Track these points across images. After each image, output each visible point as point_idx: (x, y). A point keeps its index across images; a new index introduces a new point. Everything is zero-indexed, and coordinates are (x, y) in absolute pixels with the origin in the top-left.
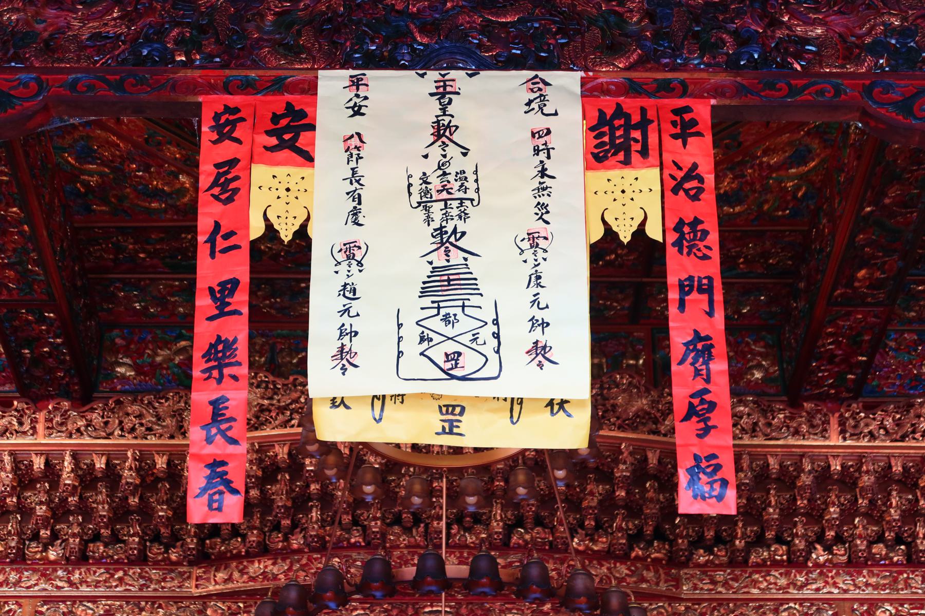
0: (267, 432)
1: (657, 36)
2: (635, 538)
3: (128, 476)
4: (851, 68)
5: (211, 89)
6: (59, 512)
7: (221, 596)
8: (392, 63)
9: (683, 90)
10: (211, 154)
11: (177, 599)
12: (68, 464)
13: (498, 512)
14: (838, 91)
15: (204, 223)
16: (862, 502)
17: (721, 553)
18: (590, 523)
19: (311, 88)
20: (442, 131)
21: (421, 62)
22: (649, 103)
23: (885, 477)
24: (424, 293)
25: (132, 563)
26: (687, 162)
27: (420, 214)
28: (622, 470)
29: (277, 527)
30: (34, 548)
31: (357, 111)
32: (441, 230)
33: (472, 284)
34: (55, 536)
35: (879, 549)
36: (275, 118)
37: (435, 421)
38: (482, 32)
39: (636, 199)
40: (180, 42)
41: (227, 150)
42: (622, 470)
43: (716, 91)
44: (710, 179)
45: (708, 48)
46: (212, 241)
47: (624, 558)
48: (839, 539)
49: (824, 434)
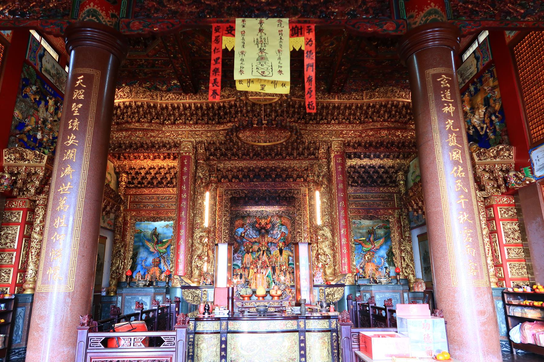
0: (230, 99)
1: (304, 11)
2: (299, 119)
3: (204, 107)
4: (343, 18)
5: (214, 22)
6: (192, 115)
7: (223, 130)
8: (251, 17)
9: (309, 22)
10: (214, 35)
11: (214, 131)
12: (193, 106)
13: (273, 114)
14: (340, 23)
15: (213, 48)
16: (341, 112)
17: (315, 121)
18: (290, 116)
19: (234, 22)
20: (261, 30)
21: (257, 17)
22: (303, 25)
23: (346, 107)
24: (257, 60)
25: (206, 124)
26: (309, 38)
27: (257, 46)
28: (297, 106)
29: (232, 117)
30: (188, 121)
31: (244, 26)
32: (261, 49)
33: (267, 59)
34: (191, 119)
35: (344, 121)
36: (227, 28)
37: (260, 88)
38: (269, 10)
39: (300, 43)
40: (208, 13)
41: (218, 34)
42: (297, 106)
43: (316, 23)
44: (314, 41)
45: (314, 13)
46: (214, 51)
47: (297, 122)
48: (337, 119)
49: (334, 99)
